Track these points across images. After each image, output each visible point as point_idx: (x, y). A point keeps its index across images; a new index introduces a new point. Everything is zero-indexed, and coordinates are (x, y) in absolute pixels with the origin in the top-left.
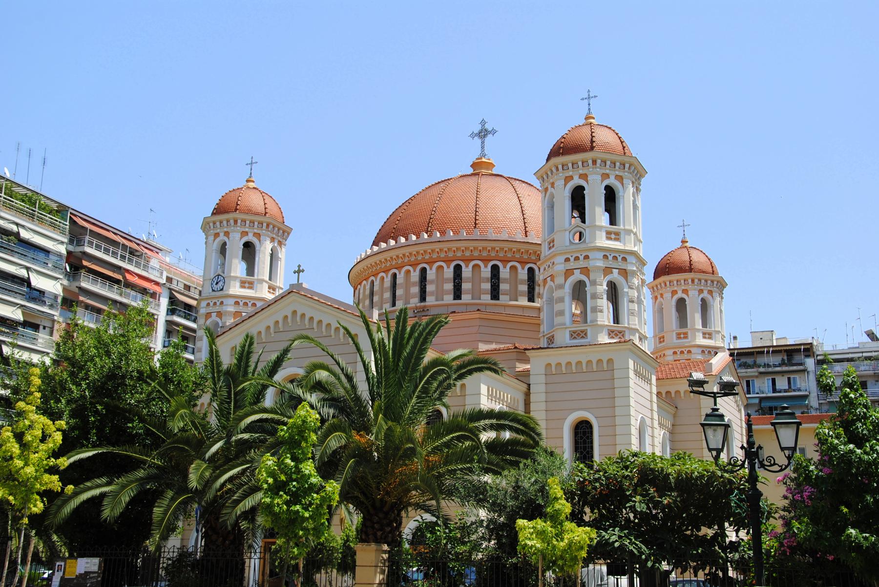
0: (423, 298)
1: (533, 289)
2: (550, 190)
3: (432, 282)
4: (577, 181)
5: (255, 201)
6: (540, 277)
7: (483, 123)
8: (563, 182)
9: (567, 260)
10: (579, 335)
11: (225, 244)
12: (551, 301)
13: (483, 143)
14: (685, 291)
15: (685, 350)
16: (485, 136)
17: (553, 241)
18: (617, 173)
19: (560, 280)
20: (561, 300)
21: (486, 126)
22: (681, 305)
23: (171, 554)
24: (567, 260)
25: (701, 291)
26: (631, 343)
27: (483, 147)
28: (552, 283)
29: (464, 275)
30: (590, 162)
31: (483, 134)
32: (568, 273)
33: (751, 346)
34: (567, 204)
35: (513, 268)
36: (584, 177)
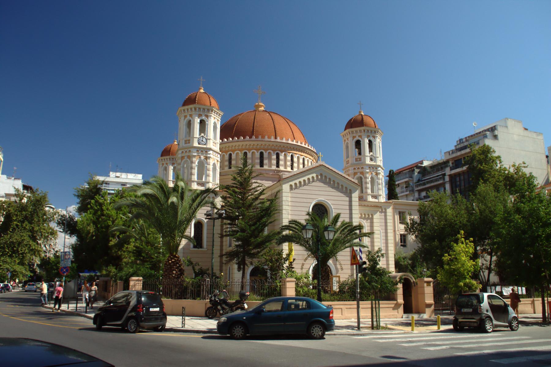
0: (278, 166)
2: (347, 141)
4: (357, 138)
9: (355, 169)
11: (190, 121)
22: (358, 144)
24: (355, 169)
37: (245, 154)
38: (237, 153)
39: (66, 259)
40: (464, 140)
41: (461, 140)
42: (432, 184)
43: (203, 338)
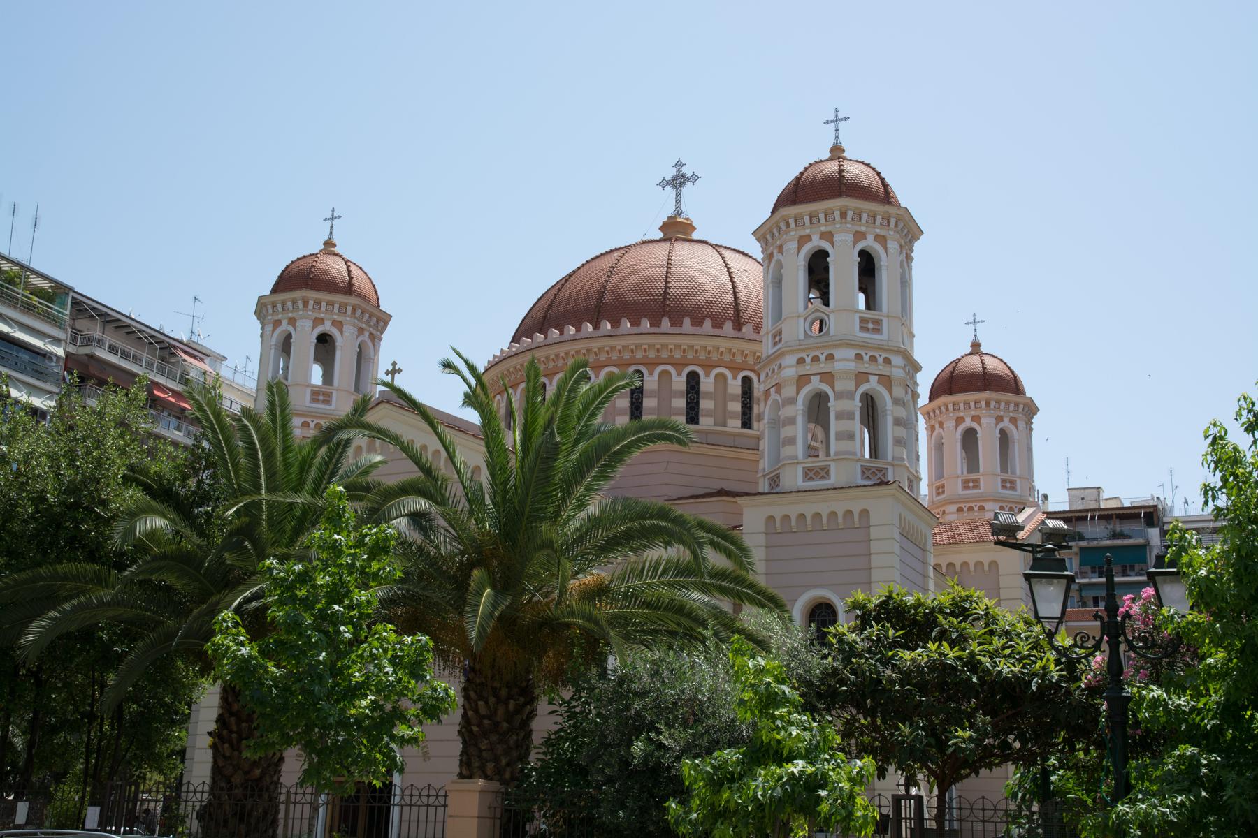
1: (750, 408)
2: (777, 256)
4: (817, 243)
5: (335, 267)
6: (758, 389)
7: (679, 165)
8: (795, 244)
10: (817, 473)
11: (289, 336)
12: (776, 424)
13: (678, 194)
14: (976, 419)
15: (976, 506)
16: (682, 184)
17: (780, 333)
18: (878, 231)
19: (789, 391)
20: (791, 421)
21: (684, 170)
22: (970, 438)
23: (199, 795)
25: (999, 419)
26: (895, 486)
27: (678, 202)
28: (778, 397)
30: (837, 214)
31: (678, 181)
32: (802, 380)
33: (1067, 509)
34: (801, 277)
35: (721, 378)
36: (828, 236)
38: (665, 374)
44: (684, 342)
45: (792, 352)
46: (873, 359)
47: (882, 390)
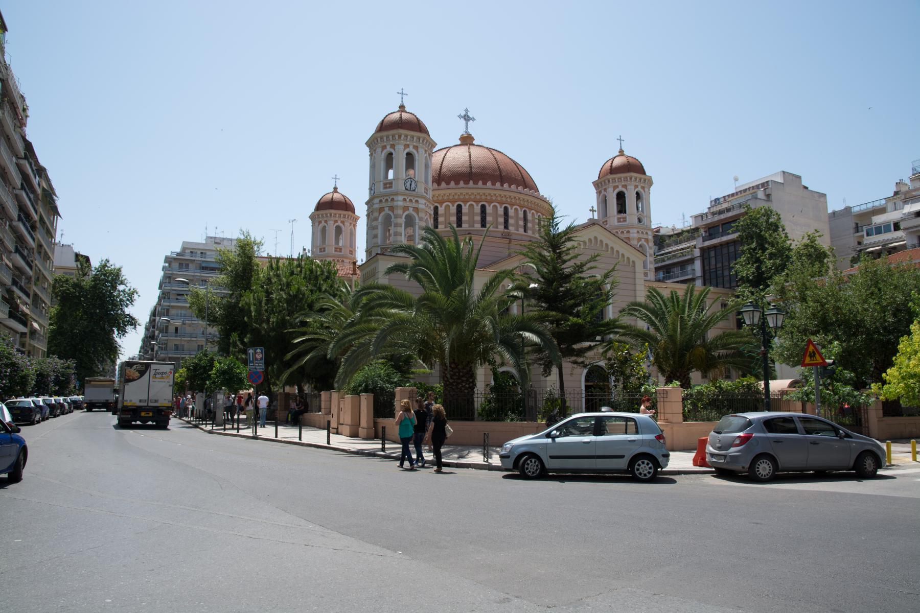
0: (506, 227)
3: (466, 214)
4: (620, 189)
11: (391, 154)
13: (467, 124)
29: (463, 211)
35: (495, 207)
37: (459, 208)
38: (447, 206)
39: (256, 359)
40: (722, 200)
41: (717, 200)
42: (676, 260)
43: (505, 477)
44: (470, 191)
45: (378, 197)
46: (411, 201)
47: (415, 214)
